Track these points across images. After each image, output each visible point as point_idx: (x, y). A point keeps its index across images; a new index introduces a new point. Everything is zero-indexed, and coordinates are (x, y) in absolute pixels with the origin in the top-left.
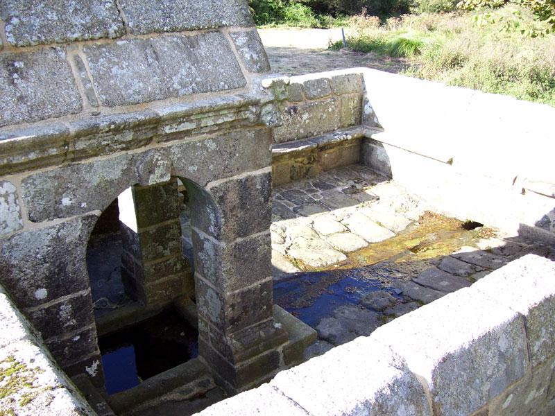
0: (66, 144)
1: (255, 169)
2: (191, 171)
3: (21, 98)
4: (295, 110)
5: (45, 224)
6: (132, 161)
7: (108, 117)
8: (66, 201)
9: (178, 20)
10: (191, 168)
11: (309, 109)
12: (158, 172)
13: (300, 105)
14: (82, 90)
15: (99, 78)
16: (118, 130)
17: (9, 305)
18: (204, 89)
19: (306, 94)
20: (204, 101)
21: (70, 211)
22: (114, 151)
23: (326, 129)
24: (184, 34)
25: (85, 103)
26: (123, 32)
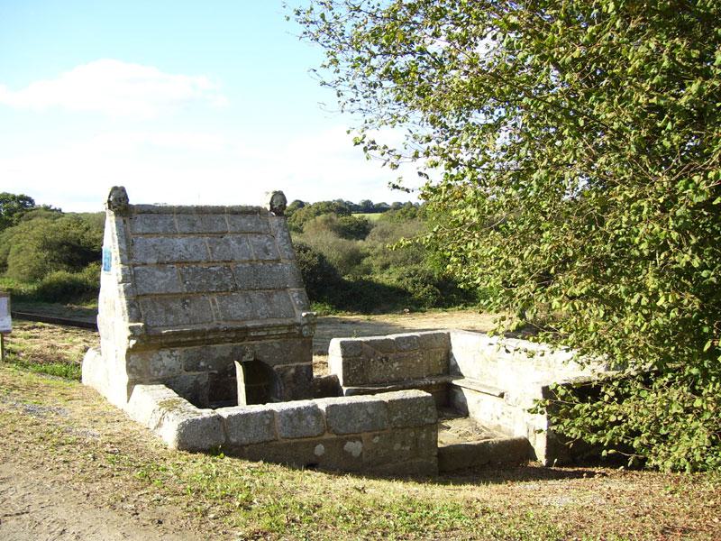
0: (204, 335)
1: (301, 362)
2: (265, 357)
3: (187, 315)
4: (387, 359)
5: (192, 373)
6: (235, 349)
7: (223, 325)
8: (202, 364)
9: (263, 285)
10: (265, 357)
11: (399, 359)
12: (247, 355)
13: (391, 356)
14: (214, 314)
15: (222, 309)
16: (228, 331)
17: (242, 205)
18: (272, 316)
19: (397, 348)
20: (271, 322)
21: (203, 369)
22: (227, 342)
23: (415, 377)
24: (266, 291)
25: (214, 319)
26: (235, 289)
